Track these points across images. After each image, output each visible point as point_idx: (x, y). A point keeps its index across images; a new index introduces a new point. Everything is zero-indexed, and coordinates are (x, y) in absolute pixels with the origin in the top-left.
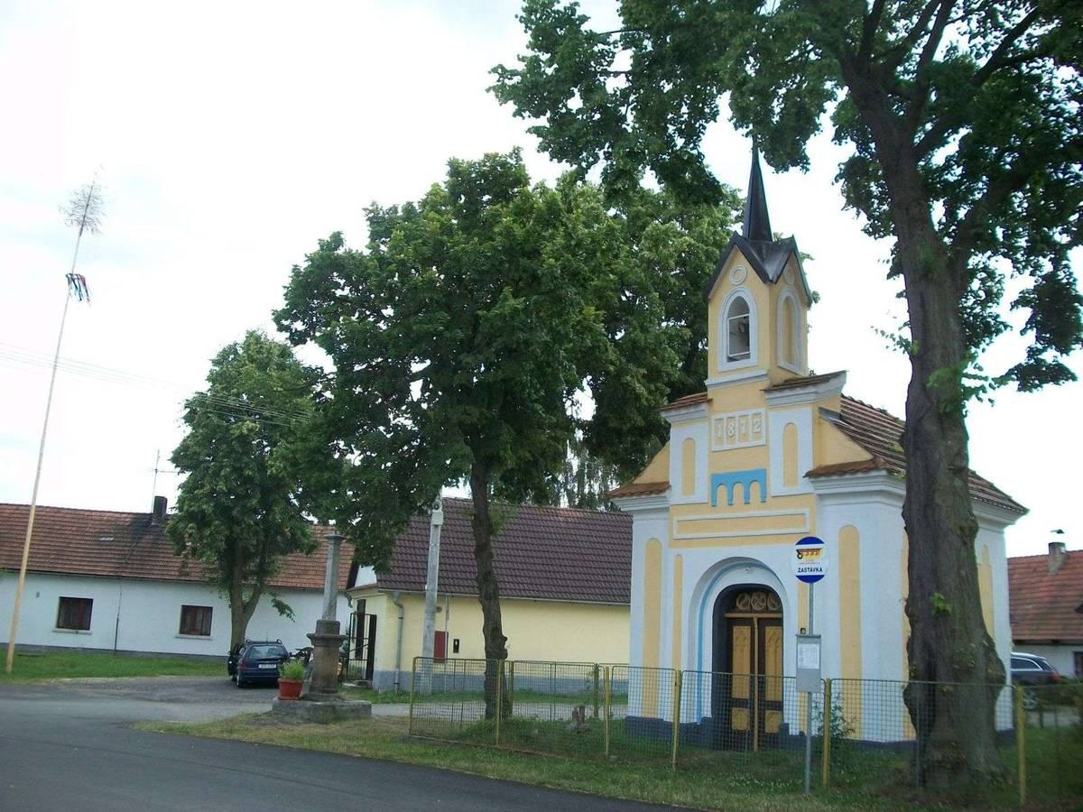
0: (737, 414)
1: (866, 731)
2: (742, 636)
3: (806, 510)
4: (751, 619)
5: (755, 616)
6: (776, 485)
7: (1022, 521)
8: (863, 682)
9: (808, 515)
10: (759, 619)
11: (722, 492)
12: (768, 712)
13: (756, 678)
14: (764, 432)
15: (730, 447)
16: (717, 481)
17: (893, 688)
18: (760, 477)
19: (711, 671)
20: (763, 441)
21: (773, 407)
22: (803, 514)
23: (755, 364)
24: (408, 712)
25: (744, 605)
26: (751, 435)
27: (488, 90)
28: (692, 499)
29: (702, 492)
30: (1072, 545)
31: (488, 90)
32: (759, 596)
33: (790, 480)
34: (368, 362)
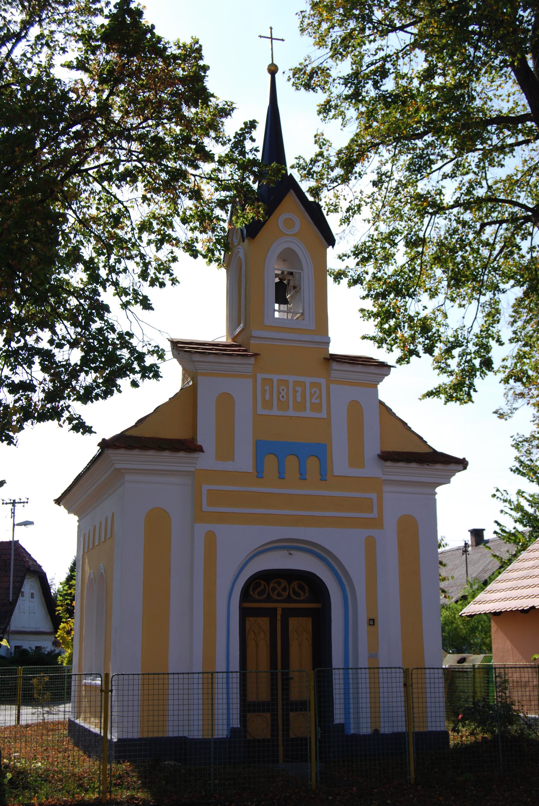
4: (275, 609)
6: (340, 464)
7: (459, 478)
8: (381, 670)
10: (283, 609)
11: (270, 462)
12: (292, 714)
13: (279, 675)
16: (262, 449)
18: (320, 452)
19: (238, 670)
24: (14, 718)
25: (259, 594)
27: (500, 382)
28: (228, 466)
29: (244, 460)
31: (500, 382)
32: (279, 584)
33: (356, 459)
34: (115, 348)
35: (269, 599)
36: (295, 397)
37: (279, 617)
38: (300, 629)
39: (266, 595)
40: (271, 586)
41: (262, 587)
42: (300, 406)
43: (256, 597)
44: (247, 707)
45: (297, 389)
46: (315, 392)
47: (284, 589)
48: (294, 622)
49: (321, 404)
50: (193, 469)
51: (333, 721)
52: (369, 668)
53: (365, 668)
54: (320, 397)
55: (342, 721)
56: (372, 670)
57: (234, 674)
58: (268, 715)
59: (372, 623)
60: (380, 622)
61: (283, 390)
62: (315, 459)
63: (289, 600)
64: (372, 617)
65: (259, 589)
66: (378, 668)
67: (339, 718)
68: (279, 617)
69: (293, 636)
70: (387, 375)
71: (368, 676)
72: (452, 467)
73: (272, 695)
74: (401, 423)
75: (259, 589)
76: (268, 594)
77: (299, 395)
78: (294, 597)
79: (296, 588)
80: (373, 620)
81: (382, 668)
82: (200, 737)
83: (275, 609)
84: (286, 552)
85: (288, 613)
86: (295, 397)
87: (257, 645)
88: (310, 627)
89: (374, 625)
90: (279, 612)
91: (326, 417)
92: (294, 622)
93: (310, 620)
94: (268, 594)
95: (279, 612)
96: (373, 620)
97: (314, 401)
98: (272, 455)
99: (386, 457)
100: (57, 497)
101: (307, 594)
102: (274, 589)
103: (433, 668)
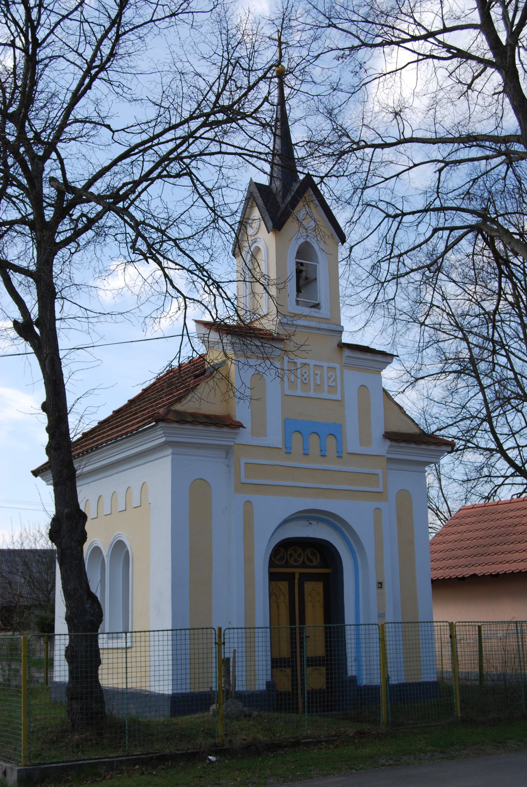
0: (312, 362)
1: (363, 636)
2: (315, 645)
3: (379, 471)
4: (293, 574)
5: (298, 571)
6: (353, 444)
8: (257, 630)
9: (381, 475)
10: (301, 574)
14: (339, 389)
15: (304, 394)
16: (292, 427)
17: (183, 637)
18: (336, 432)
20: (338, 397)
21: (347, 366)
22: (377, 475)
23: (328, 317)
26: (326, 388)
29: (274, 436)
30: (402, 624)
33: (365, 438)
35: (287, 565)
36: (315, 379)
37: (296, 581)
38: (314, 591)
39: (285, 561)
40: (289, 552)
41: (282, 553)
42: (318, 387)
43: (277, 562)
44: (276, 663)
45: (317, 372)
46: (331, 375)
47: (299, 556)
48: (309, 586)
49: (335, 387)
50: (232, 444)
51: (346, 673)
52: (245, 628)
53: (242, 628)
54: (335, 380)
55: (354, 673)
56: (248, 630)
57: (63, 637)
58: (288, 671)
59: (380, 586)
60: (386, 585)
61: (305, 372)
62: (332, 438)
63: (303, 565)
64: (380, 581)
65: (279, 556)
66: (254, 628)
67: (351, 671)
68: (296, 581)
69: (307, 598)
70: (390, 363)
71: (244, 635)
72: (444, 448)
73: (292, 652)
74: (397, 407)
75: (279, 556)
76: (287, 560)
77: (318, 377)
78: (308, 563)
79: (309, 554)
80: (381, 583)
81: (258, 628)
82: (188, 691)
83: (293, 574)
84: (306, 523)
85: (305, 578)
86: (315, 379)
87: (278, 607)
88: (321, 591)
89: (381, 587)
90: (297, 576)
91: (340, 399)
92: (309, 586)
93: (321, 584)
94: (287, 560)
95: (297, 576)
96: (381, 583)
97: (330, 384)
98: (297, 433)
99: (390, 436)
100: (34, 468)
101: (319, 560)
102: (291, 555)
103: (145, 632)
